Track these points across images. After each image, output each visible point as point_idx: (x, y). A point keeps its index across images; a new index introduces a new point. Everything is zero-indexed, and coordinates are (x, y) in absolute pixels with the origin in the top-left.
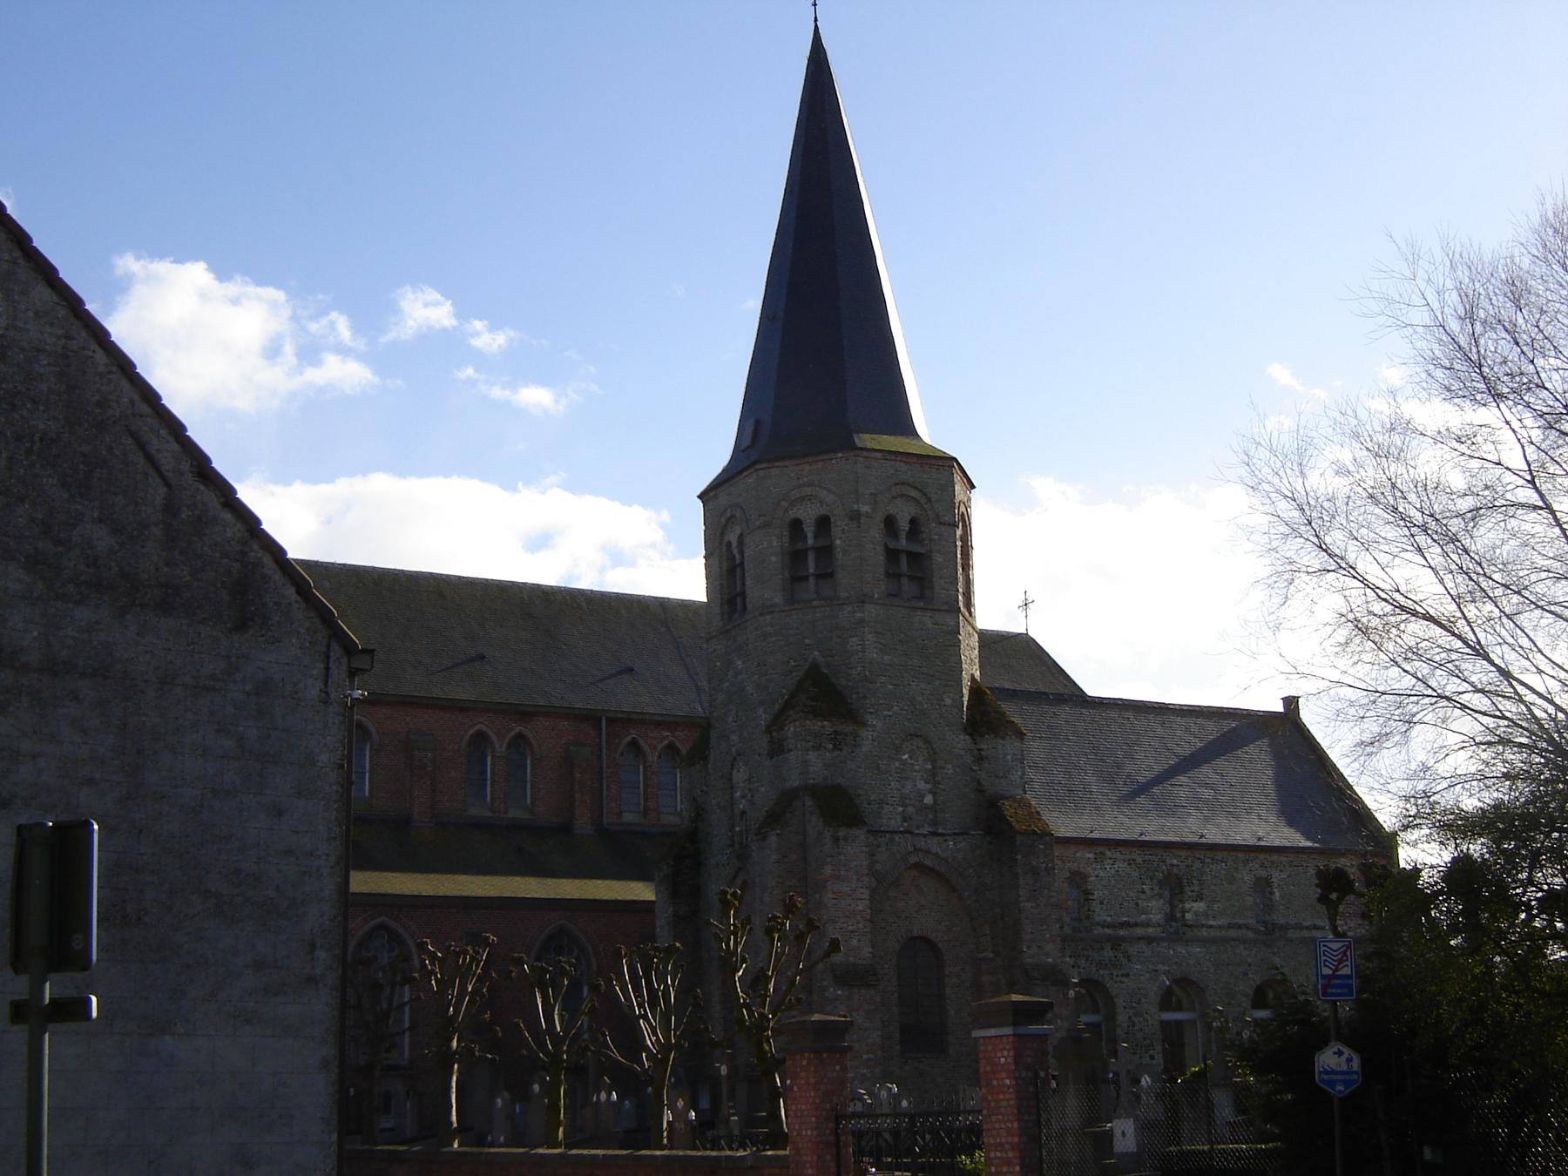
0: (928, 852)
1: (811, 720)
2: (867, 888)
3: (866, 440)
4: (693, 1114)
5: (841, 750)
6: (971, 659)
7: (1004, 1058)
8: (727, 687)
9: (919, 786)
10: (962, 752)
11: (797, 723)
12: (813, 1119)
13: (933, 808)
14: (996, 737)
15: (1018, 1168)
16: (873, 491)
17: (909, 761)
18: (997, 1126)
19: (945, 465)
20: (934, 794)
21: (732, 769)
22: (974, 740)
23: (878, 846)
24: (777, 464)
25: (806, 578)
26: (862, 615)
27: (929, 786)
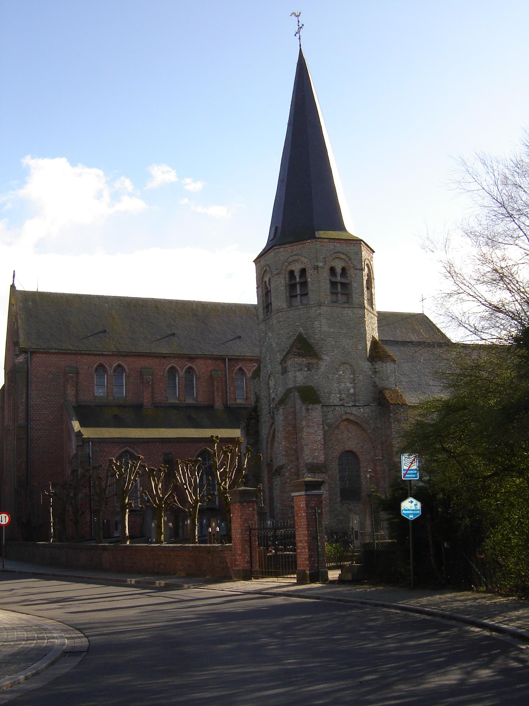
0: (351, 414)
1: (297, 358)
2: (322, 430)
3: (321, 234)
4: (218, 529)
5: (311, 371)
6: (373, 329)
7: (303, 505)
8: (266, 344)
9: (347, 385)
10: (367, 370)
11: (291, 360)
12: (240, 530)
13: (354, 395)
14: (383, 362)
15: (307, 550)
16: (324, 257)
17: (343, 374)
18: (300, 532)
19: (358, 242)
20: (354, 389)
21: (269, 380)
22: (372, 364)
23: (329, 412)
24: (283, 246)
25: (296, 296)
26: (320, 311)
27: (352, 385)
